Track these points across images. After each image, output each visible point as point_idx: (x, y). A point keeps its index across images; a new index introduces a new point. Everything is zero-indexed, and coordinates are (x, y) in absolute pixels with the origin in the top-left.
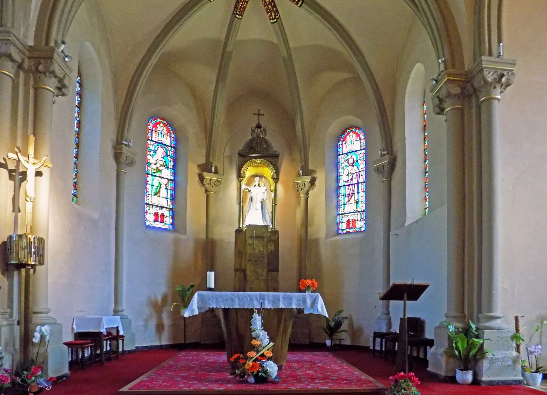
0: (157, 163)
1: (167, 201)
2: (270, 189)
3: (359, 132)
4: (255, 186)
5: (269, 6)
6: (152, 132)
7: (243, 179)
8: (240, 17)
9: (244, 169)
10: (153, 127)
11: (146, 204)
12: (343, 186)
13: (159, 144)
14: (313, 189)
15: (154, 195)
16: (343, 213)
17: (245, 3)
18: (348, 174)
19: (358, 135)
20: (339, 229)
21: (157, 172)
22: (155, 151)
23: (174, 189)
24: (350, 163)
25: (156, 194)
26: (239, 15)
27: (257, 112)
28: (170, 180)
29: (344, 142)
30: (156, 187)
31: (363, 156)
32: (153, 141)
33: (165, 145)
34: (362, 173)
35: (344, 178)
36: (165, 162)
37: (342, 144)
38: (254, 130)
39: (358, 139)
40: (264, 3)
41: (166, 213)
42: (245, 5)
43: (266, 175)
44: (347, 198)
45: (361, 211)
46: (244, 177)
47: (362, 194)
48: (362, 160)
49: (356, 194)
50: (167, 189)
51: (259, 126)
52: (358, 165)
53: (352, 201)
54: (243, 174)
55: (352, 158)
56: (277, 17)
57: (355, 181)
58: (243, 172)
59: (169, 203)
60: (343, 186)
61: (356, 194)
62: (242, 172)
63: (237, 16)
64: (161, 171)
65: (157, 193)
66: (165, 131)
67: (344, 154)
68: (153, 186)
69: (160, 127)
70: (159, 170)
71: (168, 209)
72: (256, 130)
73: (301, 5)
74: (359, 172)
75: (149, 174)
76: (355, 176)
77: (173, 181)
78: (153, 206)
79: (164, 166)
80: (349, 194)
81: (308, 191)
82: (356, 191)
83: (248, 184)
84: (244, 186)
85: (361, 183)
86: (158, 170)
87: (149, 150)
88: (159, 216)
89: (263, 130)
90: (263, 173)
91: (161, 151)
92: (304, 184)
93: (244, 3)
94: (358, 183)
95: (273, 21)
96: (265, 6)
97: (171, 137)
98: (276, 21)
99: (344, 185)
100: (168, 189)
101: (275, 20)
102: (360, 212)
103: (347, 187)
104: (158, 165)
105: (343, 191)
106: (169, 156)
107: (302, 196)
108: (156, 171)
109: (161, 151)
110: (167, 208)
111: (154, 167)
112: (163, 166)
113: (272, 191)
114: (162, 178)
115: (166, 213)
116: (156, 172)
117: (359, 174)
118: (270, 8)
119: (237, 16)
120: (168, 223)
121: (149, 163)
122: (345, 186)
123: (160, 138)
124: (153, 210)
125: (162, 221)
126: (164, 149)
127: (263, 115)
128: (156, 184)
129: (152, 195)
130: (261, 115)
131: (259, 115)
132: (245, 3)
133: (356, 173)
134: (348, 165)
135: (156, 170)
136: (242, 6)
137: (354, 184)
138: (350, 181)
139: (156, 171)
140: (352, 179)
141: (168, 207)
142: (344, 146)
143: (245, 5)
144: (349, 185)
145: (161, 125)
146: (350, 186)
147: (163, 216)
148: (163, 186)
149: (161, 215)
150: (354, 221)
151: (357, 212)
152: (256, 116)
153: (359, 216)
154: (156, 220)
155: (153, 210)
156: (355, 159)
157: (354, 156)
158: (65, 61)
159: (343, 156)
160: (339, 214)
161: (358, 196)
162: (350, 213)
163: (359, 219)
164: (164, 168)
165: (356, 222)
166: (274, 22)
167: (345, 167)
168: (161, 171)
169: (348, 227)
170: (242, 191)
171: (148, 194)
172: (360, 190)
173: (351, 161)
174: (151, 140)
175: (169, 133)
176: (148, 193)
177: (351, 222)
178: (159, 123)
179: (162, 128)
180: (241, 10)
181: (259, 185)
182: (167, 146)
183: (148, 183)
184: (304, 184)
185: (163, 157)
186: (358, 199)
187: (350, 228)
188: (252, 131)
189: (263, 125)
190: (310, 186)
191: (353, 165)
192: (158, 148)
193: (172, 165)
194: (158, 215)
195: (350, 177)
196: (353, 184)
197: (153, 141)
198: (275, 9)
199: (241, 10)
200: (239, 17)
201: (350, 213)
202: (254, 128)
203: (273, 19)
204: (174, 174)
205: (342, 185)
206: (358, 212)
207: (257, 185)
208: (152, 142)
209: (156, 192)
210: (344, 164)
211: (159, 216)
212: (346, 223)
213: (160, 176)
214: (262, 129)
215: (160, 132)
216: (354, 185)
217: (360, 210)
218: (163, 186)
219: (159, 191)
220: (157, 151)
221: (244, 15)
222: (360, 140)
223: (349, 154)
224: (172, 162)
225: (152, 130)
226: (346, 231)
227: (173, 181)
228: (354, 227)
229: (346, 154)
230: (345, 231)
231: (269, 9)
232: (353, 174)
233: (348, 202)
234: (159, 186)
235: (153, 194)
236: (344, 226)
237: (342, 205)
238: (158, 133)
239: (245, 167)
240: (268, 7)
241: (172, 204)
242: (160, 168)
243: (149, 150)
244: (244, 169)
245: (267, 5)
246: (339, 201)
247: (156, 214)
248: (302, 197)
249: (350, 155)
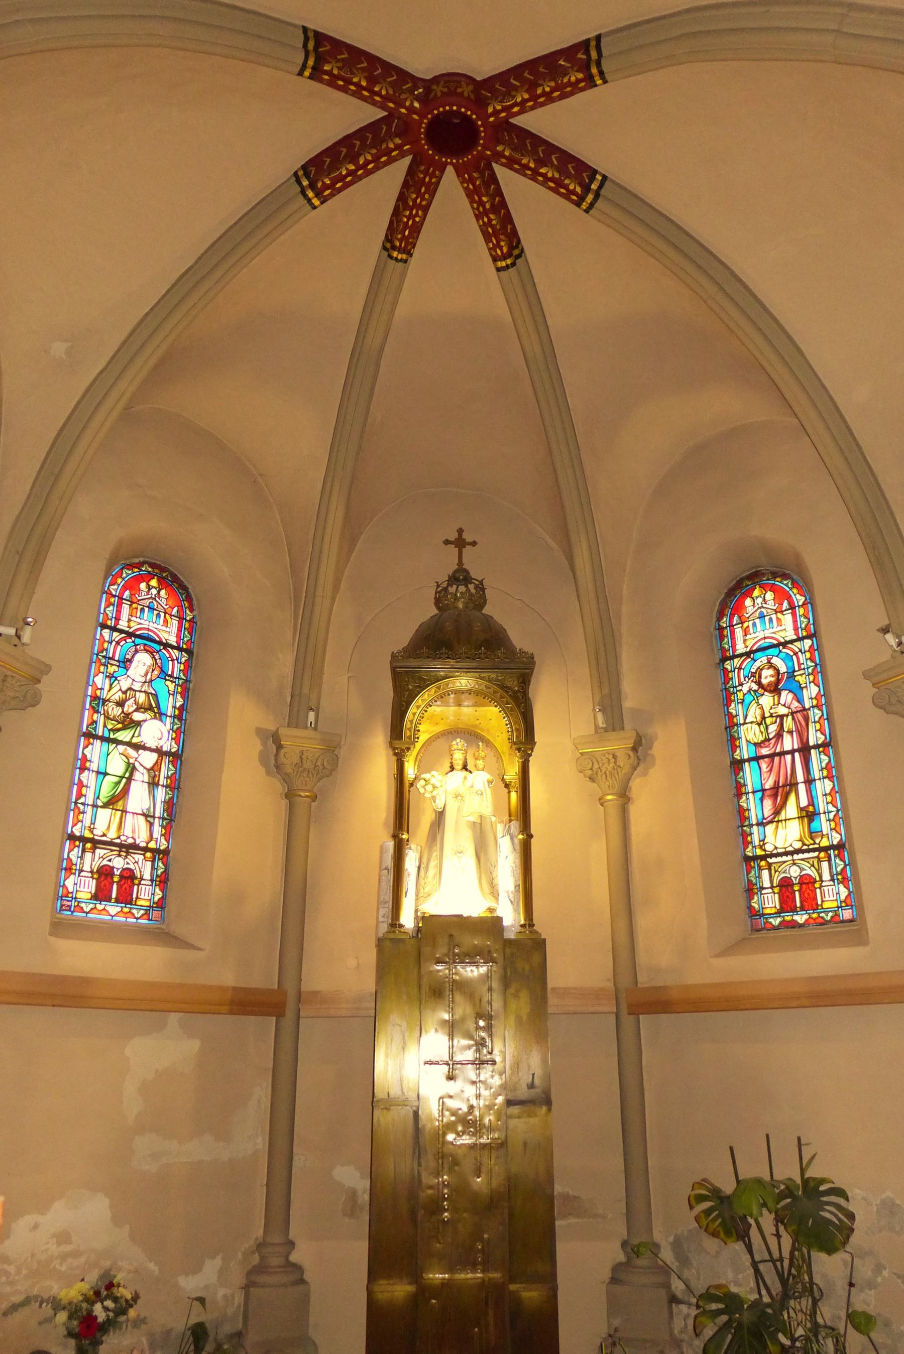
0: (126, 700)
1: (151, 825)
2: (503, 779)
3: (785, 585)
4: (452, 768)
5: (492, 216)
6: (120, 605)
7: (408, 749)
8: (404, 256)
9: (414, 714)
10: (125, 588)
11: (72, 837)
12: (750, 760)
13: (138, 641)
14: (645, 774)
15: (105, 806)
16: (759, 852)
17: (420, 213)
18: (764, 718)
19: (782, 595)
20: (754, 914)
21: (124, 728)
22: (126, 663)
23: (174, 785)
24: (764, 681)
25: (110, 803)
26: (400, 250)
27: (453, 536)
28: (169, 754)
29: (736, 620)
30: (117, 779)
31: (812, 659)
32: (121, 631)
33: (160, 643)
34: (815, 714)
35: (750, 733)
36: (156, 696)
37: (731, 626)
38: (445, 589)
39: (785, 605)
40: (478, 209)
41: (143, 867)
42: (417, 219)
43: (488, 731)
44: (768, 804)
45: (832, 847)
46: (414, 739)
47: (823, 787)
48: (810, 670)
49: (802, 788)
50: (153, 784)
51: (461, 576)
52: (794, 686)
53: (791, 809)
54: (410, 729)
55: (771, 666)
56: (516, 252)
57: (789, 743)
58: (411, 722)
59: (157, 831)
60: (750, 760)
61: (802, 788)
62: (407, 724)
63: (395, 254)
64: (139, 724)
65: (116, 800)
66: (163, 602)
67: (741, 655)
68: (106, 774)
69: (149, 588)
70: (132, 721)
71: (148, 855)
72: (452, 589)
73: (592, 205)
74: (804, 709)
75: (96, 737)
76: (789, 723)
77: (176, 757)
78: (96, 844)
79: (150, 708)
80: (776, 788)
81: (629, 779)
82: (800, 777)
83: (423, 767)
84: (410, 770)
85: (817, 747)
86: (128, 723)
87: (104, 657)
88: (116, 879)
89: (476, 587)
90: (476, 726)
91: (143, 661)
92: (614, 757)
93: (414, 212)
94: (805, 750)
95: (504, 264)
96: (478, 217)
97: (181, 619)
98: (513, 264)
99: (753, 755)
100: (157, 785)
101: (509, 261)
102: (825, 849)
103: (764, 765)
104: (130, 707)
105: (751, 776)
106: (172, 676)
107: (609, 797)
108: (120, 726)
109: (143, 661)
110: (146, 849)
111: (116, 711)
112: (146, 710)
113: (507, 786)
114: (138, 747)
115: (143, 867)
116: (119, 730)
117: (807, 719)
118: (494, 222)
119: (395, 254)
120: (147, 904)
121: (99, 698)
122: (757, 758)
123: (148, 622)
124: (91, 861)
125: (126, 898)
126: (157, 657)
127: (474, 544)
128: (117, 766)
129: (95, 806)
130: (470, 544)
131: (460, 543)
132: (420, 213)
133: (792, 713)
134: (760, 691)
135: (122, 723)
136: (410, 222)
137: (792, 752)
138: (773, 741)
139: (120, 726)
140: (779, 736)
141: (152, 845)
142: (739, 632)
143: (417, 219)
144: (771, 756)
145: (154, 583)
146: (777, 759)
147: (129, 877)
148: (141, 776)
149: (801, 883)
150: (807, 882)
151: (814, 850)
152: (453, 550)
153: (825, 865)
154: (101, 895)
155: (91, 861)
156: (783, 669)
157: (776, 661)
158: (628, 1259)
159: (737, 662)
160: (748, 859)
161: (809, 792)
162: (786, 854)
163: (826, 876)
164: (147, 716)
165: (817, 885)
166: (507, 267)
167: (748, 698)
168: (139, 724)
169: (787, 905)
170: (407, 784)
171: (83, 804)
172: (816, 773)
173: (767, 676)
174: (114, 629)
175: (176, 609)
176: (82, 800)
177: (796, 888)
178: (151, 576)
179: (154, 591)
180: (407, 233)
181: (465, 767)
182: (166, 645)
183: (88, 764)
184: (614, 757)
185: (151, 681)
186: (811, 802)
187: (794, 910)
188: (440, 592)
189: (473, 574)
190: (636, 763)
191: (775, 689)
192: (136, 652)
193: (178, 705)
194: (113, 874)
195: (773, 729)
196: (788, 752)
197: (121, 631)
198: (509, 227)
199: (407, 233)
200: (399, 257)
201: (786, 854)
202: (445, 585)
203: (504, 258)
204: (178, 734)
205: (746, 757)
206: (820, 849)
207: (459, 764)
208: (115, 634)
209: (113, 796)
210: (745, 688)
211: (116, 879)
212: (776, 890)
213: (135, 740)
214: (471, 587)
215: (147, 602)
216: (788, 758)
217: (825, 843)
218: (141, 776)
219: (126, 791)
220: (130, 661)
221: (416, 252)
222: (792, 607)
223: (758, 655)
224: (179, 697)
225: (121, 598)
226: (779, 920)
227: (176, 757)
228: (810, 903)
229: (748, 654)
230: (776, 922)
231: (493, 227)
232: (782, 717)
233: (777, 812)
234: (127, 775)
235: (100, 803)
236: (770, 901)
237: (751, 826)
238: (140, 607)
239: (418, 707)
240: (490, 220)
241: (167, 836)
242: (137, 716)
243: (104, 657)
244: (414, 714)
245: (486, 213)
246: (742, 814)
247: (104, 874)
248: (609, 801)
249: (761, 659)
